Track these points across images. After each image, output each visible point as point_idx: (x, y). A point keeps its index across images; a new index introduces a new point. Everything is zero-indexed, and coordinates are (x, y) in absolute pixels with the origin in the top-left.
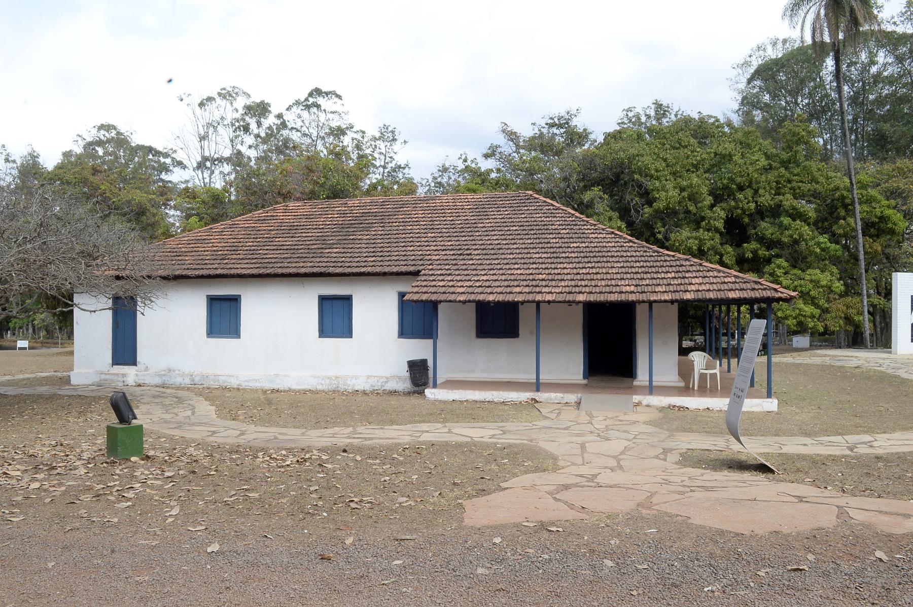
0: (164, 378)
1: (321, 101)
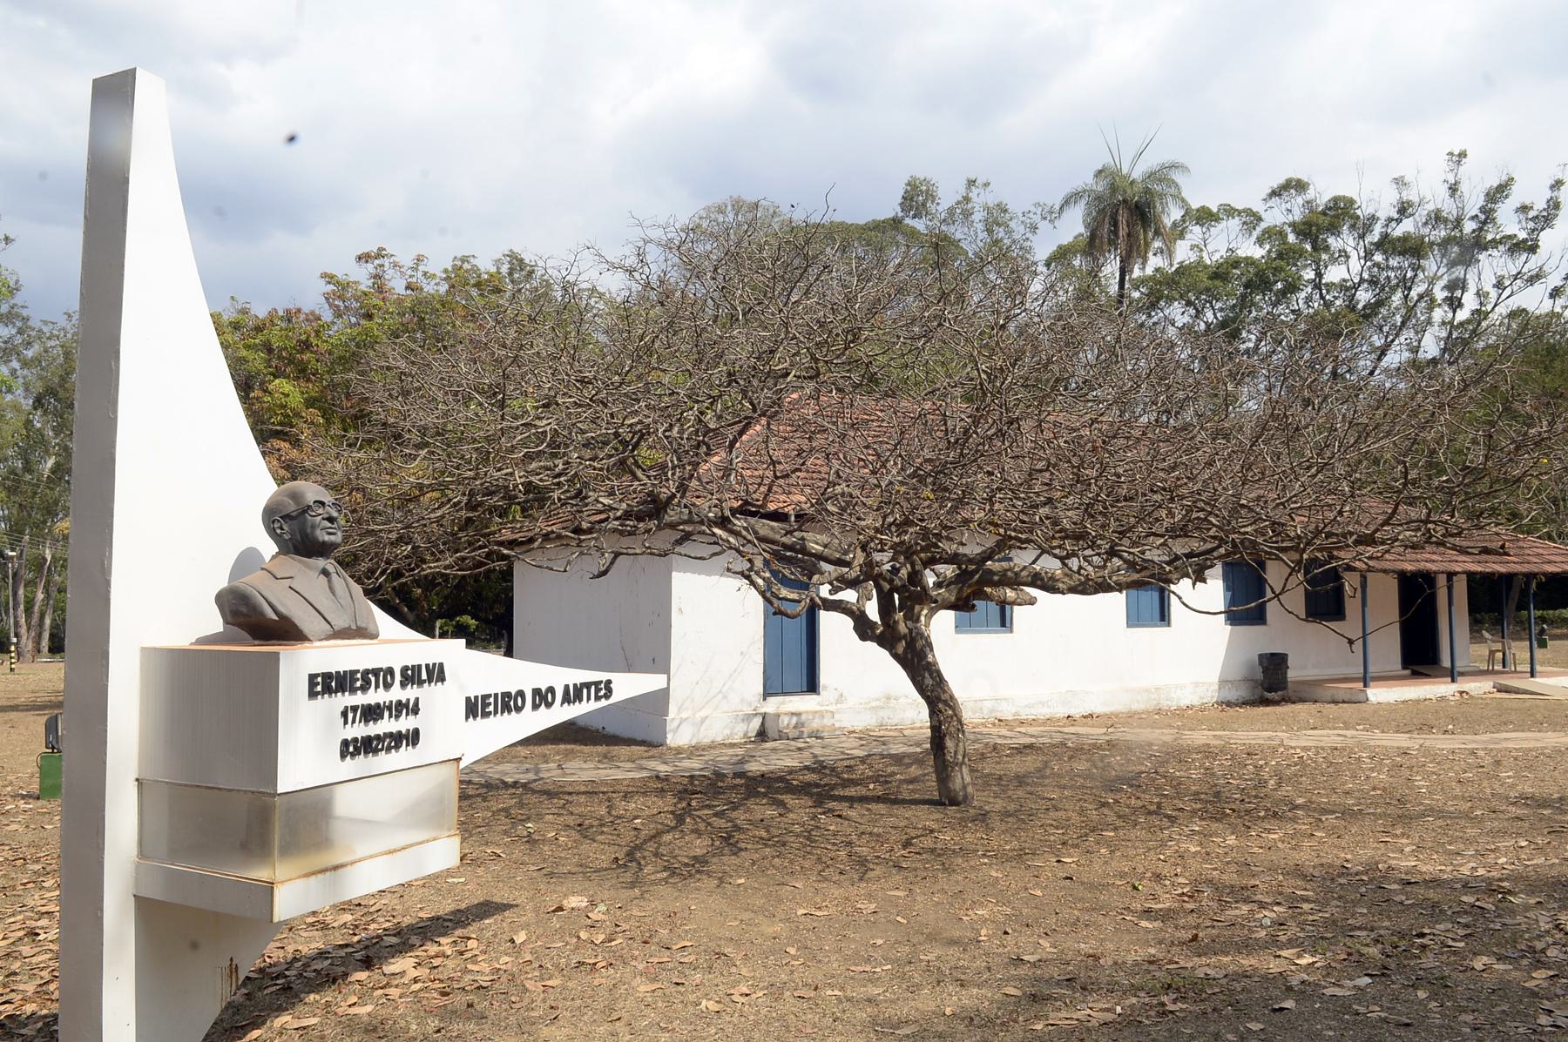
0: (882, 713)
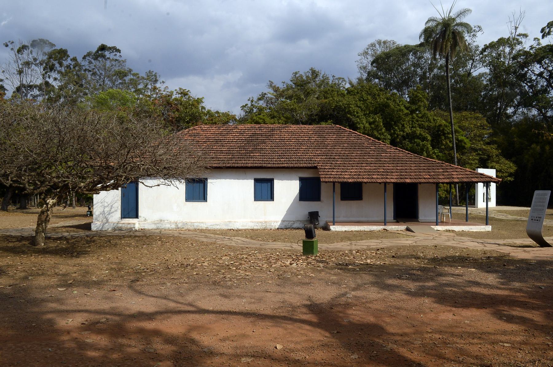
0: (158, 225)
1: (107, 53)
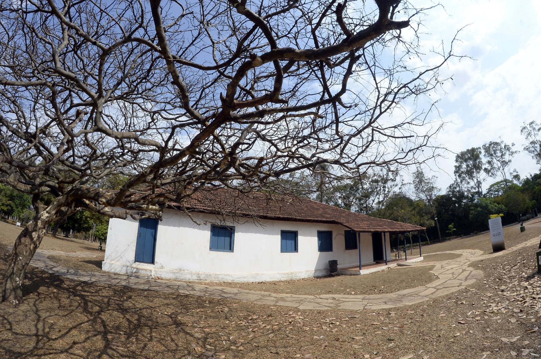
0: (177, 275)
